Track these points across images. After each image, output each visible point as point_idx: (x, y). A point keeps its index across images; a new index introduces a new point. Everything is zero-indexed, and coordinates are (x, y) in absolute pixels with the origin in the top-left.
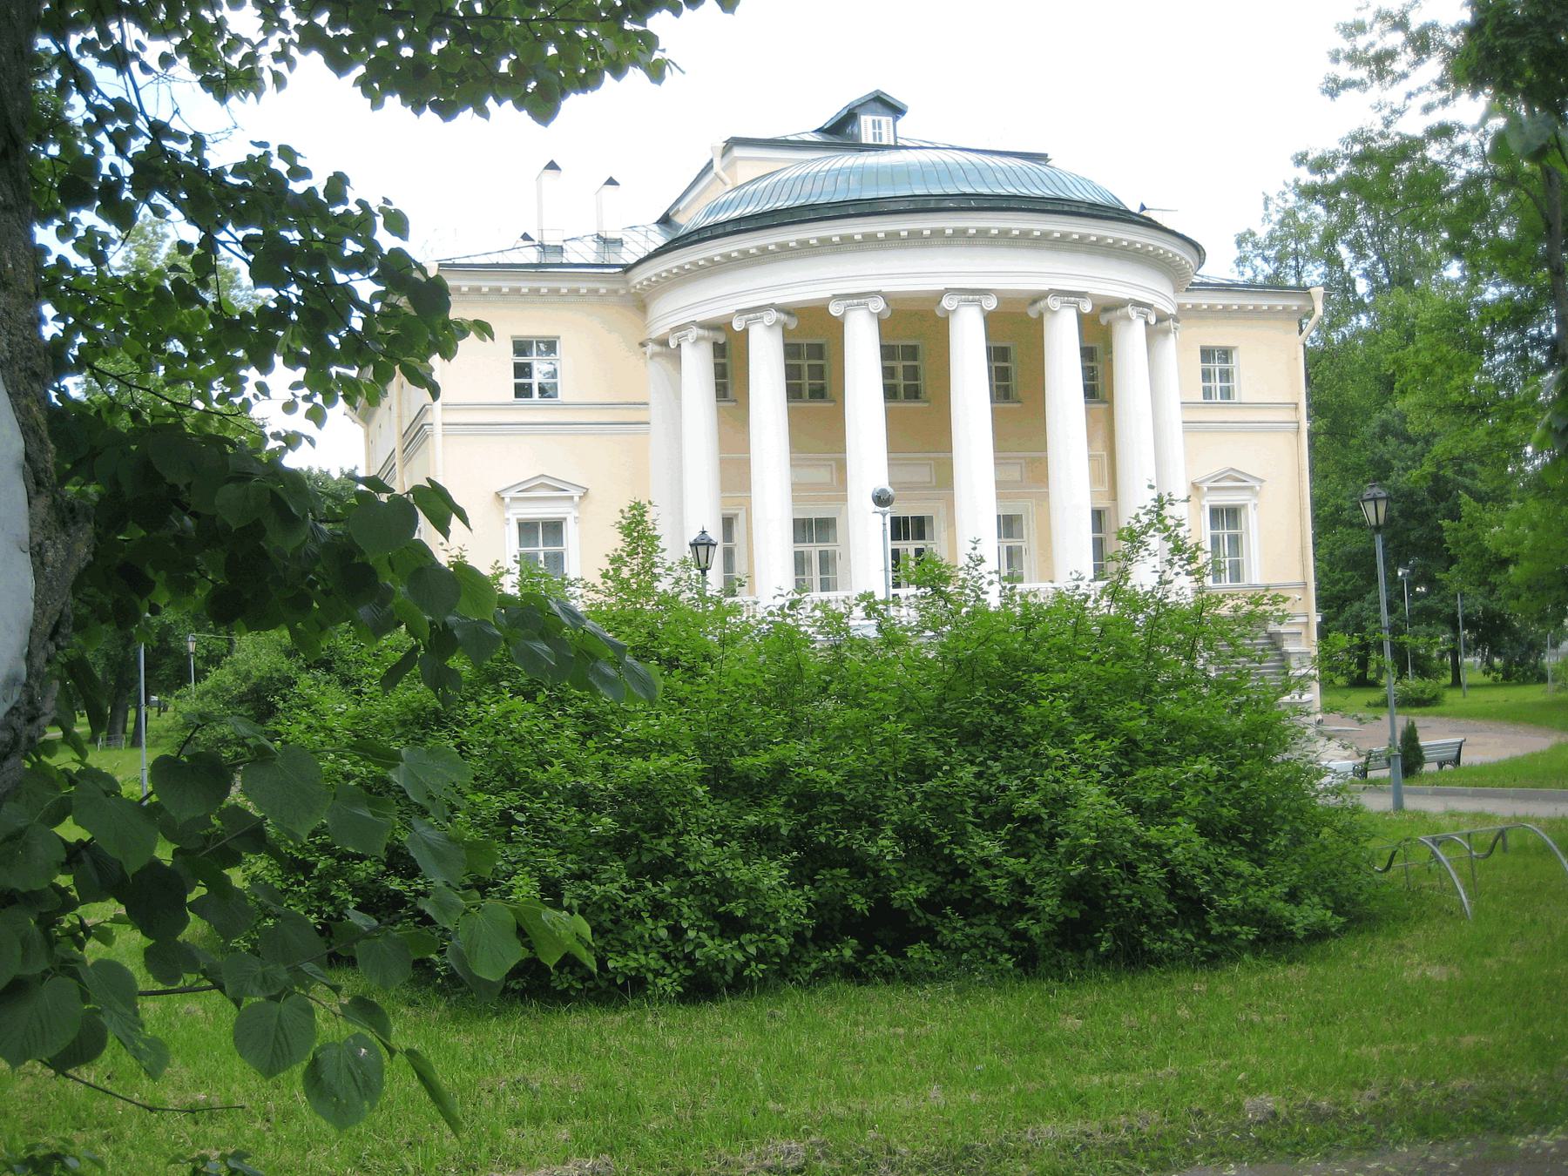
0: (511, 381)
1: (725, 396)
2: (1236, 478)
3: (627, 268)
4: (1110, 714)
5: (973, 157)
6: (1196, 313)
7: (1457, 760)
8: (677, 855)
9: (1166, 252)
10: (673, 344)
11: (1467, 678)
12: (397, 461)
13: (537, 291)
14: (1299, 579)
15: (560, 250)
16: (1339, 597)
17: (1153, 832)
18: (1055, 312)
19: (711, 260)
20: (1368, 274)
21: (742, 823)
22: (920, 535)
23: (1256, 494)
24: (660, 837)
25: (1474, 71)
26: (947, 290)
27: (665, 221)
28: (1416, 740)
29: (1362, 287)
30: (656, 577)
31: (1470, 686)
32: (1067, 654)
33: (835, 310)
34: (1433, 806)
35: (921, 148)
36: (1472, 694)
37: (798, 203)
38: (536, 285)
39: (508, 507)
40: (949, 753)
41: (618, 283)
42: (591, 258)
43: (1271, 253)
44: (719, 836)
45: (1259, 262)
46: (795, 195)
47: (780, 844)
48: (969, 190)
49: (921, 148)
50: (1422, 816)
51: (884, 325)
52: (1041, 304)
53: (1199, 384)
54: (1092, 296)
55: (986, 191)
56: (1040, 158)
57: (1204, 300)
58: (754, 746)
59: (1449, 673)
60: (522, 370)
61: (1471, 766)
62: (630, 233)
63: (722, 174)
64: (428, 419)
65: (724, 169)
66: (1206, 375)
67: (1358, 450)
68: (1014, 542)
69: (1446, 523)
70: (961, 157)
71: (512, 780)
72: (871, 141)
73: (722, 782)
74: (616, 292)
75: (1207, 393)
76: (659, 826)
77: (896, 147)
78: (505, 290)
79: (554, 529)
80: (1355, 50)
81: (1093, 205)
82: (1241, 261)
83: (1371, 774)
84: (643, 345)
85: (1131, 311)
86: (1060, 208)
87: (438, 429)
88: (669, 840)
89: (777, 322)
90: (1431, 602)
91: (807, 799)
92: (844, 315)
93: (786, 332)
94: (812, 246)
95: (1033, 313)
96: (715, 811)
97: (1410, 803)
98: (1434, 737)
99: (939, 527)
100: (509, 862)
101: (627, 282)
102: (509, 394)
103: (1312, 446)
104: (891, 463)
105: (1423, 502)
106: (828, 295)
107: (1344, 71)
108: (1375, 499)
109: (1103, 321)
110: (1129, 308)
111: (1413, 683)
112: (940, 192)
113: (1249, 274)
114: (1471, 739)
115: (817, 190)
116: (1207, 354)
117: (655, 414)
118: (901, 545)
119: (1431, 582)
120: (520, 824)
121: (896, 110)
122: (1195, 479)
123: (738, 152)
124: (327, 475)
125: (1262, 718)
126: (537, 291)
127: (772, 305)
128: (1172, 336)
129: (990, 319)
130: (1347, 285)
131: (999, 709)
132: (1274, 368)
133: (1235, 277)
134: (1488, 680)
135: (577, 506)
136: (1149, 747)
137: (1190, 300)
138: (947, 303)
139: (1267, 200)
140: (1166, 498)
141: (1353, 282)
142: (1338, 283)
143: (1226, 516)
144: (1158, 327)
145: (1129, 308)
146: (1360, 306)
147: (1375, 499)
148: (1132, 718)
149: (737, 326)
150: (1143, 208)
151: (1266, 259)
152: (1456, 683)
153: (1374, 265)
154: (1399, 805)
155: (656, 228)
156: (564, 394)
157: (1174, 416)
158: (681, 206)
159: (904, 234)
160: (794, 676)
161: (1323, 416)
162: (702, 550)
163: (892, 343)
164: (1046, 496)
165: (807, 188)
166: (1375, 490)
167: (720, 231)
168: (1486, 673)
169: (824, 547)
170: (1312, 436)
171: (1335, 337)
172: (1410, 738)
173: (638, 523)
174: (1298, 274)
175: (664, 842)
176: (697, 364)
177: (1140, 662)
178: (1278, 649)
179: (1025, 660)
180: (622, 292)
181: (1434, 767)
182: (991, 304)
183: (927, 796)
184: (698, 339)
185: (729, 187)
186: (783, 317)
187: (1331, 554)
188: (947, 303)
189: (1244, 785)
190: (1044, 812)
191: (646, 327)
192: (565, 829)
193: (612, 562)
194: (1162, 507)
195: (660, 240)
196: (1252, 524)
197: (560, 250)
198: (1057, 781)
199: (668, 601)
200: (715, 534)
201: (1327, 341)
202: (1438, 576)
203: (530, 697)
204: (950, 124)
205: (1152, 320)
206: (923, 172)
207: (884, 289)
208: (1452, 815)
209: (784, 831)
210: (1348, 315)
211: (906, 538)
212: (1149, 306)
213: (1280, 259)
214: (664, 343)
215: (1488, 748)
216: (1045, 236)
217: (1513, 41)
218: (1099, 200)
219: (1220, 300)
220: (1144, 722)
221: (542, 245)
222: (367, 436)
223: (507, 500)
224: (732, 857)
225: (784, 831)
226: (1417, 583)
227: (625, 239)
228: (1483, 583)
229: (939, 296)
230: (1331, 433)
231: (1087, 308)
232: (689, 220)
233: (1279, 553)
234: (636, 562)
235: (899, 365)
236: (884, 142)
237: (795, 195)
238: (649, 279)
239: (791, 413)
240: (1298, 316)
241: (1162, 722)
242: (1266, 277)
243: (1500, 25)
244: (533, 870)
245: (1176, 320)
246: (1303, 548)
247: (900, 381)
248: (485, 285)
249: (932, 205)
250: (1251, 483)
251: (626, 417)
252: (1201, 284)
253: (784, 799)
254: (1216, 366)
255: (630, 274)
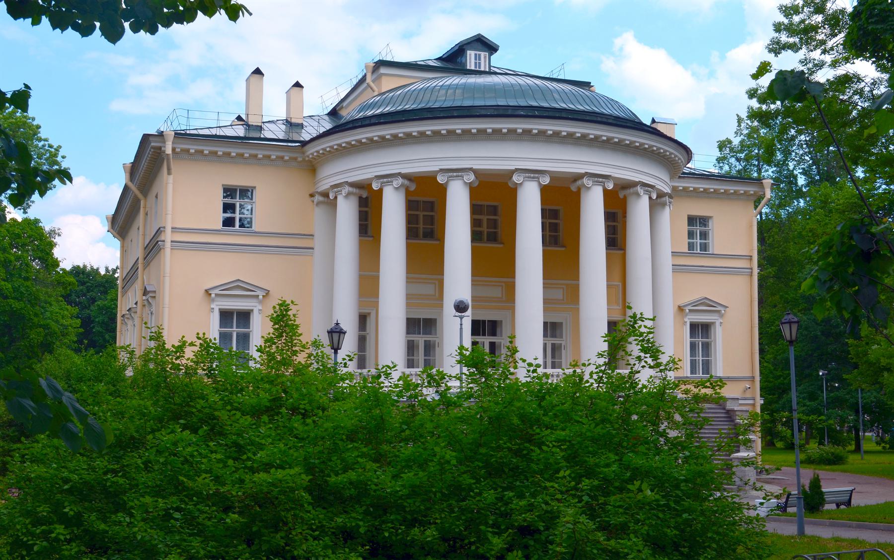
0: (221, 216)
1: (366, 233)
2: (708, 305)
3: (304, 144)
4: (591, 461)
5: (538, 82)
6: (686, 193)
7: (848, 503)
8: (287, 545)
9: (665, 151)
10: (331, 196)
11: (866, 446)
12: (140, 266)
13: (242, 155)
14: (748, 374)
15: (260, 128)
16: (773, 389)
17: (612, 542)
18: (589, 188)
19: (359, 141)
20: (805, 173)
21: (333, 524)
22: (493, 333)
23: (722, 316)
24: (277, 532)
25: (855, 43)
26: (517, 170)
27: (334, 113)
28: (820, 487)
29: (801, 181)
30: (295, 353)
31: (867, 452)
32: (567, 418)
33: (441, 179)
34: (826, 533)
35: (506, 74)
36: (866, 457)
37: (420, 107)
38: (241, 151)
39: (213, 300)
40: (478, 481)
41: (296, 152)
42: (281, 136)
43: (742, 156)
44: (317, 533)
45: (733, 160)
46: (418, 101)
47: (360, 540)
48: (535, 104)
49: (506, 74)
50: (816, 540)
51: (474, 192)
52: (579, 183)
53: (686, 240)
54: (615, 179)
55: (545, 105)
56: (586, 85)
57: (691, 184)
58: (345, 471)
59: (853, 442)
60: (228, 207)
61: (858, 507)
62: (309, 120)
63: (372, 84)
64: (162, 238)
65: (373, 81)
66: (691, 235)
67: (796, 289)
68: (556, 341)
69: (850, 341)
70: (530, 81)
71: (179, 488)
72: (473, 68)
73: (323, 495)
74: (296, 159)
75: (691, 246)
76: (276, 525)
77: (490, 73)
78: (206, 152)
79: (244, 317)
80: (791, 24)
81: (617, 118)
82: (719, 160)
83: (789, 510)
84: (312, 196)
85: (639, 189)
86: (595, 119)
87: (168, 245)
88: (283, 534)
89: (402, 185)
90: (840, 394)
91: (382, 507)
92: (447, 183)
93: (408, 193)
94: (442, 135)
95: (573, 188)
96: (315, 515)
97: (809, 530)
98: (833, 485)
99: (506, 330)
100: (167, 545)
101: (303, 153)
102: (219, 226)
103: (760, 286)
104: (474, 283)
105: (837, 326)
106: (437, 169)
107: (784, 38)
108: (790, 323)
109: (621, 196)
110: (639, 188)
111: (829, 448)
112: (515, 104)
113: (726, 168)
114: (858, 488)
115: (433, 98)
116: (692, 220)
117: (318, 243)
118: (479, 339)
119: (841, 380)
120: (177, 520)
121: (491, 48)
122: (690, 306)
123: (383, 70)
124: (96, 271)
125: (700, 468)
126: (242, 155)
127: (399, 174)
128: (667, 208)
129: (545, 191)
130: (791, 179)
131: (517, 453)
132: (736, 232)
133: (716, 171)
134: (879, 448)
135: (260, 302)
136: (617, 484)
137: (681, 184)
138: (516, 178)
139: (740, 120)
140: (639, 316)
141: (795, 177)
142: (786, 177)
143: (701, 330)
144: (658, 203)
145: (639, 188)
146: (800, 194)
147: (790, 323)
148: (609, 464)
149: (375, 186)
150: (653, 121)
151: (738, 160)
152: (858, 449)
153: (810, 166)
154: (801, 532)
155: (327, 118)
156: (255, 227)
157: (667, 262)
158: (345, 104)
159: (489, 131)
160: (378, 422)
161: (772, 265)
162: (335, 336)
163: (479, 203)
164: (577, 310)
165: (427, 97)
166: (790, 316)
167: (367, 122)
168: (878, 443)
169: (428, 338)
170: (762, 281)
171: (783, 213)
172: (816, 484)
173: (284, 316)
174: (759, 171)
175: (278, 536)
176: (347, 212)
177: (617, 426)
178: (733, 421)
179: (538, 420)
180: (300, 159)
181: (834, 506)
182: (546, 180)
183: (462, 511)
184: (348, 195)
185: (376, 93)
186: (406, 182)
187: (775, 358)
188: (516, 178)
189: (685, 516)
190: (541, 526)
191: (315, 183)
192: (209, 523)
193: (266, 341)
194: (635, 323)
195: (328, 125)
196: (719, 336)
197: (260, 128)
198: (547, 503)
199: (300, 371)
200: (349, 324)
201: (778, 216)
202: (845, 376)
203: (195, 431)
204: (525, 58)
205: (654, 196)
206: (505, 90)
207: (475, 167)
208: (837, 540)
209: (362, 530)
210: (792, 199)
211: (484, 335)
212: (652, 187)
213: (747, 159)
214: (325, 195)
215: (868, 495)
216: (570, 135)
217: (879, 27)
218: (622, 115)
219: (701, 185)
220: (614, 467)
221: (248, 125)
222: (122, 247)
223: (213, 295)
224: (326, 547)
225: (362, 530)
226: (833, 380)
227: (305, 123)
228: (876, 382)
229: (512, 173)
230: (777, 277)
231: (610, 186)
232: (348, 113)
233: (736, 355)
234: (280, 343)
235: (484, 218)
236: (482, 69)
237: (418, 101)
238: (318, 152)
239: (409, 247)
240: (755, 198)
241: (627, 468)
242: (739, 171)
243: (871, 16)
244: (184, 551)
245: (670, 196)
246: (752, 354)
247: (484, 229)
248: (193, 148)
249: (510, 112)
250: (719, 308)
251: (297, 244)
252: (690, 173)
253: (364, 508)
254: (698, 229)
255: (306, 148)
